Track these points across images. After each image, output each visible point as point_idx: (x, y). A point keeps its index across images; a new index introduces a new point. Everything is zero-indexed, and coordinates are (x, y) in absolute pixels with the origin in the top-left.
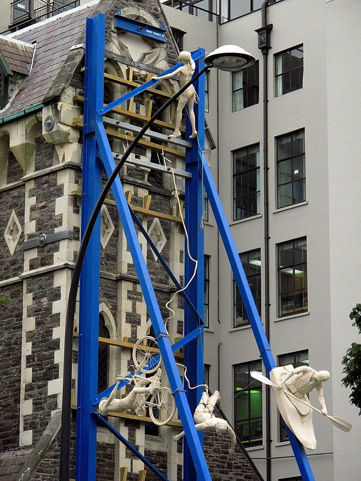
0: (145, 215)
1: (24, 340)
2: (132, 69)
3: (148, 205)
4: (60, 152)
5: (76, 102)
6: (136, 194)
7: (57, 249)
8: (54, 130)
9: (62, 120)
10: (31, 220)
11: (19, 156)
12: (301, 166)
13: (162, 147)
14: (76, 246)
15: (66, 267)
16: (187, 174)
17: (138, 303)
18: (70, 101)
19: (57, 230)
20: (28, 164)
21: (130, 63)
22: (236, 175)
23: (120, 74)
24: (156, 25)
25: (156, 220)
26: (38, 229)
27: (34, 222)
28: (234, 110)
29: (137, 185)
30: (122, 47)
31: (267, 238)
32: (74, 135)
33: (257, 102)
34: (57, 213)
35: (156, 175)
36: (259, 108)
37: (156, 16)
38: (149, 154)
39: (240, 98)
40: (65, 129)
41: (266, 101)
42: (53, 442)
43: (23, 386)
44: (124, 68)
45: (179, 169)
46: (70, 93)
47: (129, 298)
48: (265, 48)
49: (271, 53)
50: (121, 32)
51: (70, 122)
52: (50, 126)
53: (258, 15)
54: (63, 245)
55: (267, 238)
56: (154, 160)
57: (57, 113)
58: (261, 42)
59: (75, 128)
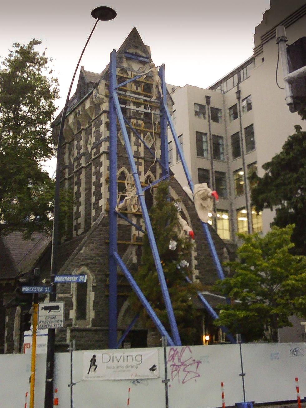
0: (142, 131)
1: (92, 185)
2: (133, 73)
3: (143, 126)
4: (101, 107)
5: (106, 85)
6: (137, 122)
7: (101, 146)
8: (97, 97)
9: (99, 93)
10: (94, 136)
11: (89, 112)
12: (253, 137)
13: (148, 103)
14: (108, 144)
15: (104, 152)
16: (161, 114)
17: (140, 167)
18: (104, 85)
19: (101, 138)
20: (92, 115)
21: (133, 71)
22: (233, 144)
23: (128, 75)
24: (144, 55)
25: (148, 133)
26: (96, 140)
27: (95, 137)
28: (231, 121)
29: (138, 119)
30: (129, 65)
31: (244, 164)
32: (106, 99)
33: (237, 118)
34: (101, 132)
35: (147, 115)
36: (238, 119)
37: (145, 53)
38: (143, 106)
39: (232, 117)
40: (101, 97)
41: (240, 116)
42: (99, 225)
43: (92, 204)
44: (129, 73)
45: (158, 112)
46: (104, 82)
47: (136, 165)
48: (239, 98)
49: (241, 100)
50: (129, 59)
51: (104, 93)
52: (96, 96)
53: (236, 88)
54: (103, 143)
55: (244, 164)
56: (145, 108)
57: (98, 90)
58: (237, 97)
59: (106, 96)
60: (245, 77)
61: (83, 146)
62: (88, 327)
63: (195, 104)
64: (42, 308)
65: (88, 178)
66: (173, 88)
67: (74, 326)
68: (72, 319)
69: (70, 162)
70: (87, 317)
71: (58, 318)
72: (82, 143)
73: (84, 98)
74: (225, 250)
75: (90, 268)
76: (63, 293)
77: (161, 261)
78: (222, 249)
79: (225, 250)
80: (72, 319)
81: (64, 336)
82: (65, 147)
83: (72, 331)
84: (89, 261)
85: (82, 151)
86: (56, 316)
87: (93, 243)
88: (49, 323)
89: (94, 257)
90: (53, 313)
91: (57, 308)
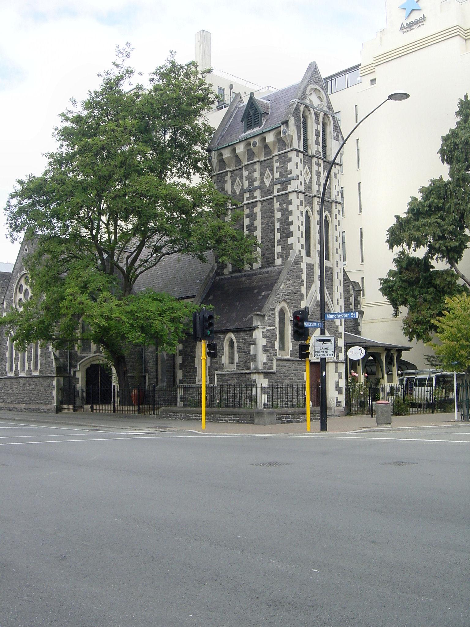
8: (287, 134)
20: (274, 149)
27: (278, 173)
60: (334, 91)
61: (258, 178)
62: (288, 357)
63: (467, 94)
64: (317, 340)
65: (268, 214)
66: (230, 85)
67: (279, 356)
68: (276, 350)
69: (234, 192)
70: (286, 348)
71: (330, 349)
72: (256, 175)
73: (232, 119)
74: (351, 287)
75: (287, 303)
76: (270, 326)
77: (395, 304)
78: (349, 286)
79: (351, 287)
80: (276, 350)
81: (272, 365)
82: (227, 175)
83: (277, 360)
84: (287, 297)
85: (256, 184)
86: (328, 347)
87: (288, 280)
88: (323, 353)
89: (290, 293)
90: (326, 345)
91: (329, 341)
